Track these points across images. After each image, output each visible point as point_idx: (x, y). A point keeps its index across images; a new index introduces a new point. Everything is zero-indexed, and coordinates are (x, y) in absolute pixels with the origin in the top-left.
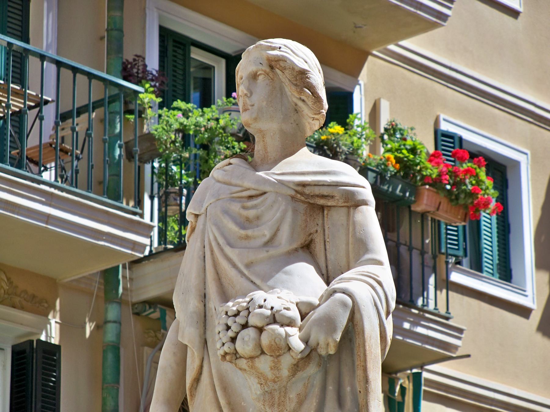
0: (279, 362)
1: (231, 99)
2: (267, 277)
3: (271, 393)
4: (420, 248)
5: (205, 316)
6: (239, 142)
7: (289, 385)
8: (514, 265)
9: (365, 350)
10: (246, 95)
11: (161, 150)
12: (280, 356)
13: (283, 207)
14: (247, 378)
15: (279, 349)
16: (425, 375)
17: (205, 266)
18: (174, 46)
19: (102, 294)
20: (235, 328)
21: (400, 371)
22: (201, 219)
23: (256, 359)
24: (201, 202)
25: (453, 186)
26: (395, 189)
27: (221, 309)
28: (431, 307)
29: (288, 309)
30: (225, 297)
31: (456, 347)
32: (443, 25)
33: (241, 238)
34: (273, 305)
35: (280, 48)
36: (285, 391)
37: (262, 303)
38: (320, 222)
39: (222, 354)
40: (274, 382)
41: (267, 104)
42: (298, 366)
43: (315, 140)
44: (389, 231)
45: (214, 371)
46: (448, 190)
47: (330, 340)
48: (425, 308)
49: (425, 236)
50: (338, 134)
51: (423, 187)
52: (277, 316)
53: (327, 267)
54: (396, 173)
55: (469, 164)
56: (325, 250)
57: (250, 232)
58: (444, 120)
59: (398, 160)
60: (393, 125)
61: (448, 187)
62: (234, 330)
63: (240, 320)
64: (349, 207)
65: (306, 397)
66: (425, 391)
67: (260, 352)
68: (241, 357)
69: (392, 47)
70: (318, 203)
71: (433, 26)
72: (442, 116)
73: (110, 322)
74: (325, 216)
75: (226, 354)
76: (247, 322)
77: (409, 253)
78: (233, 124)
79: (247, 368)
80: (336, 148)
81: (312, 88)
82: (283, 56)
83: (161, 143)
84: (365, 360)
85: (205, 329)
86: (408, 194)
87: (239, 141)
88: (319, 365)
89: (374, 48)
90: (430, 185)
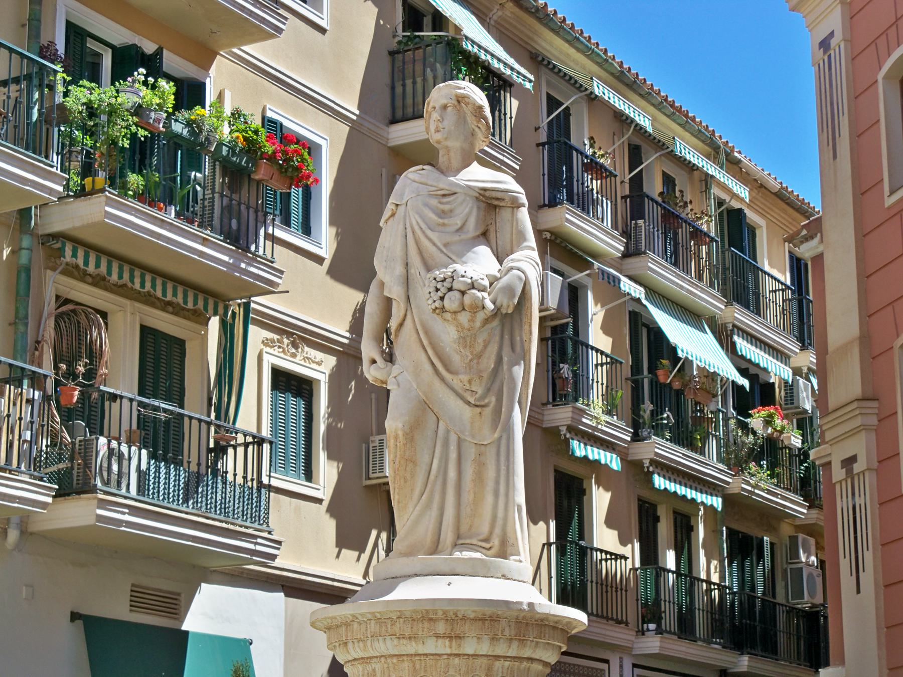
4: (255, 207)
6: (132, 116)
8: (312, 224)
11: (71, 118)
13: (470, 205)
15: (478, 307)
16: (253, 305)
18: (75, 36)
19: (18, 227)
20: (443, 290)
22: (401, 209)
24: (402, 195)
25: (284, 161)
26: (241, 161)
27: (429, 276)
28: (261, 252)
29: (482, 279)
30: (429, 269)
31: (278, 285)
33: (439, 225)
36: (474, 337)
37: (464, 274)
38: (494, 217)
39: (434, 308)
40: (469, 330)
47: (511, 303)
48: (257, 253)
55: (296, 146)
57: (446, 221)
58: (270, 109)
59: (245, 139)
61: (281, 162)
63: (447, 284)
64: (513, 208)
66: (252, 318)
68: (446, 311)
69: (235, 50)
71: (271, 36)
72: (268, 106)
73: (24, 249)
75: (436, 308)
76: (452, 287)
79: (450, 319)
81: (485, 118)
83: (71, 112)
87: (132, 115)
89: (222, 49)
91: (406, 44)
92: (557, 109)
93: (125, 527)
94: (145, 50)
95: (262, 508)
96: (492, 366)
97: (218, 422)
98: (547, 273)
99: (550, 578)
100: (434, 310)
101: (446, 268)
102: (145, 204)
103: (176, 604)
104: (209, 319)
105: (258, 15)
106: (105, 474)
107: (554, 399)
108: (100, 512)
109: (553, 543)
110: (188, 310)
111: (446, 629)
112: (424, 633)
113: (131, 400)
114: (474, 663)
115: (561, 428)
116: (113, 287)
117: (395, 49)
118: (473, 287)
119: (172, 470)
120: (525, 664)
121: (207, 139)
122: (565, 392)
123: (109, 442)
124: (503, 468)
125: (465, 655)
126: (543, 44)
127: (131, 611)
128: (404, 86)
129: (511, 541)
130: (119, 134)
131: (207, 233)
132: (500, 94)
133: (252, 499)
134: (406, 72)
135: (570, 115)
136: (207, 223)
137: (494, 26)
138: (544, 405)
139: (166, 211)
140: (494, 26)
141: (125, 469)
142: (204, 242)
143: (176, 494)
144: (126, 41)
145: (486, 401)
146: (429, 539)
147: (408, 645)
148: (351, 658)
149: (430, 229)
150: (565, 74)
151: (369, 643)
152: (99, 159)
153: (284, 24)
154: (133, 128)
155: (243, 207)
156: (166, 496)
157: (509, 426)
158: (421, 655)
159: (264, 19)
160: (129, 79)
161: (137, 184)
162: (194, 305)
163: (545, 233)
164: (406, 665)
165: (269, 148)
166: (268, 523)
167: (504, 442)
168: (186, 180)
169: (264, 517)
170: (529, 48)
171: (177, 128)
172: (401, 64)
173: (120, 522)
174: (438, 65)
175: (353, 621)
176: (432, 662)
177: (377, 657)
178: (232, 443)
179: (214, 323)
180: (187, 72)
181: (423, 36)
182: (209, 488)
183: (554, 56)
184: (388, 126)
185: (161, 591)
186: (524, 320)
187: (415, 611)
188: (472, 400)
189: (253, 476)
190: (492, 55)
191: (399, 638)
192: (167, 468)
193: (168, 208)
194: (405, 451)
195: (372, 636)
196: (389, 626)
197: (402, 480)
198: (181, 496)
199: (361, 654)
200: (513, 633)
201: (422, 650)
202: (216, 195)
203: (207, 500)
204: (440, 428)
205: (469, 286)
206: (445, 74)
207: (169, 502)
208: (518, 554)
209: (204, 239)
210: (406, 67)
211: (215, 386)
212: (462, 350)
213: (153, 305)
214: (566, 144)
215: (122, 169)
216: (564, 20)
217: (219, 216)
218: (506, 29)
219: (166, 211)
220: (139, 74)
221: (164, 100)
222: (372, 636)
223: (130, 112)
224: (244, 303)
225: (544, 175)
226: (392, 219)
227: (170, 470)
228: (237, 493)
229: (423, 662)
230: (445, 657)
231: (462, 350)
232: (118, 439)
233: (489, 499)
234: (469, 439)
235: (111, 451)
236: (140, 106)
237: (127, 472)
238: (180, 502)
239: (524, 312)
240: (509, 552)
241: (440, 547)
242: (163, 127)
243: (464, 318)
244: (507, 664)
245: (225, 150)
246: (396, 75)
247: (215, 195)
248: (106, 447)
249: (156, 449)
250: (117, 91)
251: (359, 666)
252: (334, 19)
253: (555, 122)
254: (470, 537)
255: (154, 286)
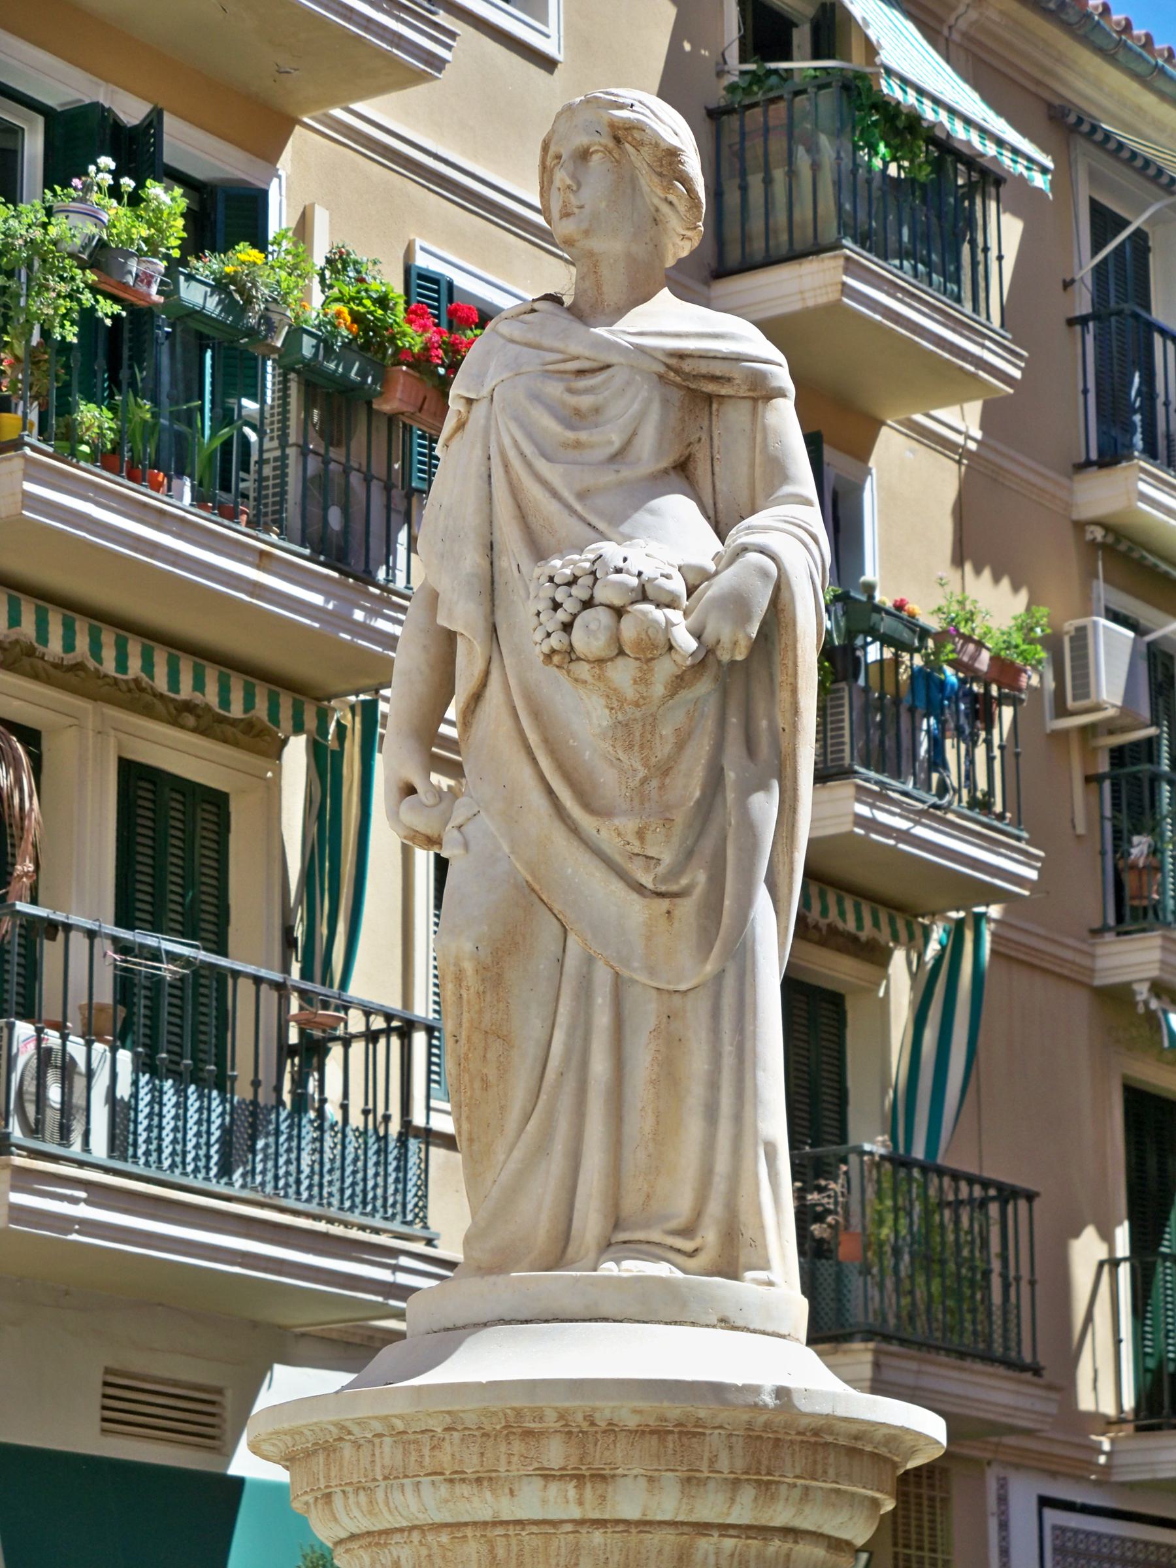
0: (651, 670)
1: (71, 190)
2: (618, 518)
3: (627, 725)
4: (385, 478)
5: (493, 582)
6: (83, 269)
7: (660, 711)
9: (795, 657)
10: (569, 187)
12: (652, 659)
13: (644, 394)
14: (584, 697)
15: (655, 647)
17: (490, 492)
20: (570, 606)
21: (336, 696)
22: (479, 410)
23: (609, 663)
24: (480, 378)
26: (348, 369)
27: (537, 571)
28: (400, 583)
29: (668, 577)
30: (539, 554)
32: (437, 78)
33: (566, 445)
34: (641, 569)
35: (632, 106)
36: (652, 722)
37: (621, 564)
38: (705, 424)
39: (546, 649)
40: (637, 705)
41: (607, 206)
42: (682, 679)
43: (213, 273)
44: (332, 444)
45: (512, 682)
46: (440, 376)
48: (391, 585)
49: (394, 457)
50: (255, 264)
51: (398, 368)
52: (647, 587)
53: (715, 504)
54: (351, 340)
56: (713, 474)
57: (583, 436)
58: (422, 249)
59: (357, 318)
60: (341, 253)
61: (442, 371)
62: (570, 611)
63: (579, 592)
64: (755, 400)
65: (690, 734)
67: (616, 652)
68: (579, 659)
69: (338, 113)
70: (704, 389)
71: (420, 78)
72: (419, 242)
74: (714, 413)
75: (553, 651)
76: (592, 597)
77: (364, 485)
78: (74, 236)
80: (250, 289)
81: (686, 181)
82: (638, 120)
84: (795, 675)
85: (493, 605)
86: (370, 380)
87: (83, 269)
88: (716, 679)
89: (305, 111)
90: (408, 366)
91: (747, 91)
92: (1115, 235)
93: (78, 1232)
94: (122, 116)
95: (410, 1185)
96: (697, 794)
97: (307, 985)
98: (1095, 624)
99: (1118, 1342)
100: (548, 657)
101: (581, 551)
102: (119, 474)
103: (212, 1415)
104: (285, 742)
105: (385, 28)
106: (31, 1109)
107: (1120, 919)
108: (18, 1198)
109: (1125, 1259)
110: (234, 722)
111: (567, 1457)
112: (513, 1467)
113: (91, 934)
114: (641, 1542)
115: (1136, 987)
116: (51, 670)
117: (723, 103)
118: (644, 598)
119: (192, 1098)
120: (776, 1545)
121: (265, 318)
122: (1145, 903)
123: (39, 1031)
124: (728, 1048)
125: (618, 1522)
126: (1080, 85)
127: (104, 1431)
128: (744, 189)
129: (749, 1233)
130: (51, 312)
131: (271, 541)
132: (972, 204)
133: (386, 1164)
134: (749, 155)
135: (1148, 249)
136: (270, 517)
137: (960, 45)
138: (1097, 932)
139: (169, 489)
140: (960, 45)
141: (78, 1099)
142: (263, 560)
143: (202, 1153)
144: (78, 96)
145: (684, 881)
146: (542, 1234)
147: (476, 1500)
148: (343, 1535)
149: (544, 455)
150: (1134, 155)
151: (380, 1494)
152: (9, 371)
153: (449, 47)
154: (87, 298)
155: (355, 479)
156: (178, 1159)
157: (744, 944)
158: (507, 1523)
159: (401, 37)
160: (76, 182)
161: (100, 427)
162: (246, 711)
163: (1092, 528)
164: (473, 1548)
165: (413, 339)
166: (424, 1220)
167: (730, 982)
168: (225, 416)
169: (416, 1205)
170: (1046, 95)
171: (193, 294)
172: (737, 139)
173: (65, 1223)
174: (824, 140)
175: (341, 1439)
176: (537, 1542)
177: (401, 1530)
178: (340, 1032)
179: (296, 752)
180: (228, 168)
181: (789, 71)
182: (282, 1139)
183: (1104, 110)
184: (707, 284)
185: (176, 1383)
186: (780, 677)
187: (488, 1413)
188: (647, 880)
189: (387, 1107)
190: (952, 111)
191: (451, 1481)
192: (181, 1092)
193: (175, 482)
194: (480, 1012)
195: (386, 1478)
196: (426, 1451)
197: (477, 1084)
198: (215, 1158)
199: (364, 1524)
200: (740, 1464)
201: (509, 1510)
202: (292, 452)
203: (276, 1167)
204: (568, 952)
205: (633, 596)
206: (839, 158)
207: (185, 1174)
208: (765, 1266)
209: (262, 553)
210: (748, 144)
211: (299, 901)
212: (621, 755)
213: (147, 711)
214: (1136, 316)
215: (64, 393)
216: (1128, 27)
217: (299, 500)
218: (991, 51)
219: (169, 489)
220: (99, 170)
221: (160, 231)
222: (386, 1478)
223: (79, 259)
224: (364, 702)
225: (1085, 391)
226: (459, 435)
227: (186, 1098)
228: (350, 1149)
229: (514, 1541)
230: (569, 1527)
231: (621, 755)
232: (61, 1027)
233: (694, 1128)
234: (641, 977)
235: (44, 1056)
236: (102, 245)
237: (83, 1103)
238: (213, 1173)
239: (777, 658)
240: (743, 1260)
241: (571, 1250)
242: (159, 292)
243: (622, 673)
244: (729, 1543)
245: (308, 344)
246: (725, 166)
247: (289, 451)
248: (32, 1047)
249: (153, 1049)
250: (49, 212)
251: (362, 1552)
252: (574, 34)
253: (1111, 266)
254: (647, 1225)
255: (148, 666)
